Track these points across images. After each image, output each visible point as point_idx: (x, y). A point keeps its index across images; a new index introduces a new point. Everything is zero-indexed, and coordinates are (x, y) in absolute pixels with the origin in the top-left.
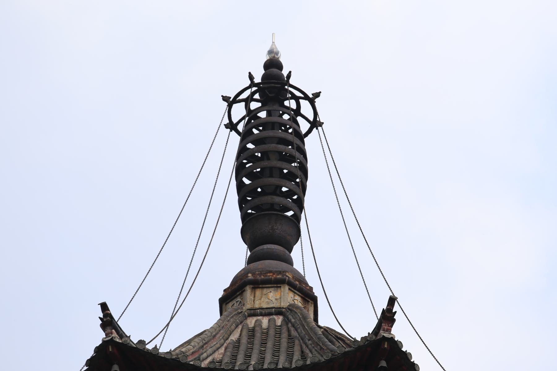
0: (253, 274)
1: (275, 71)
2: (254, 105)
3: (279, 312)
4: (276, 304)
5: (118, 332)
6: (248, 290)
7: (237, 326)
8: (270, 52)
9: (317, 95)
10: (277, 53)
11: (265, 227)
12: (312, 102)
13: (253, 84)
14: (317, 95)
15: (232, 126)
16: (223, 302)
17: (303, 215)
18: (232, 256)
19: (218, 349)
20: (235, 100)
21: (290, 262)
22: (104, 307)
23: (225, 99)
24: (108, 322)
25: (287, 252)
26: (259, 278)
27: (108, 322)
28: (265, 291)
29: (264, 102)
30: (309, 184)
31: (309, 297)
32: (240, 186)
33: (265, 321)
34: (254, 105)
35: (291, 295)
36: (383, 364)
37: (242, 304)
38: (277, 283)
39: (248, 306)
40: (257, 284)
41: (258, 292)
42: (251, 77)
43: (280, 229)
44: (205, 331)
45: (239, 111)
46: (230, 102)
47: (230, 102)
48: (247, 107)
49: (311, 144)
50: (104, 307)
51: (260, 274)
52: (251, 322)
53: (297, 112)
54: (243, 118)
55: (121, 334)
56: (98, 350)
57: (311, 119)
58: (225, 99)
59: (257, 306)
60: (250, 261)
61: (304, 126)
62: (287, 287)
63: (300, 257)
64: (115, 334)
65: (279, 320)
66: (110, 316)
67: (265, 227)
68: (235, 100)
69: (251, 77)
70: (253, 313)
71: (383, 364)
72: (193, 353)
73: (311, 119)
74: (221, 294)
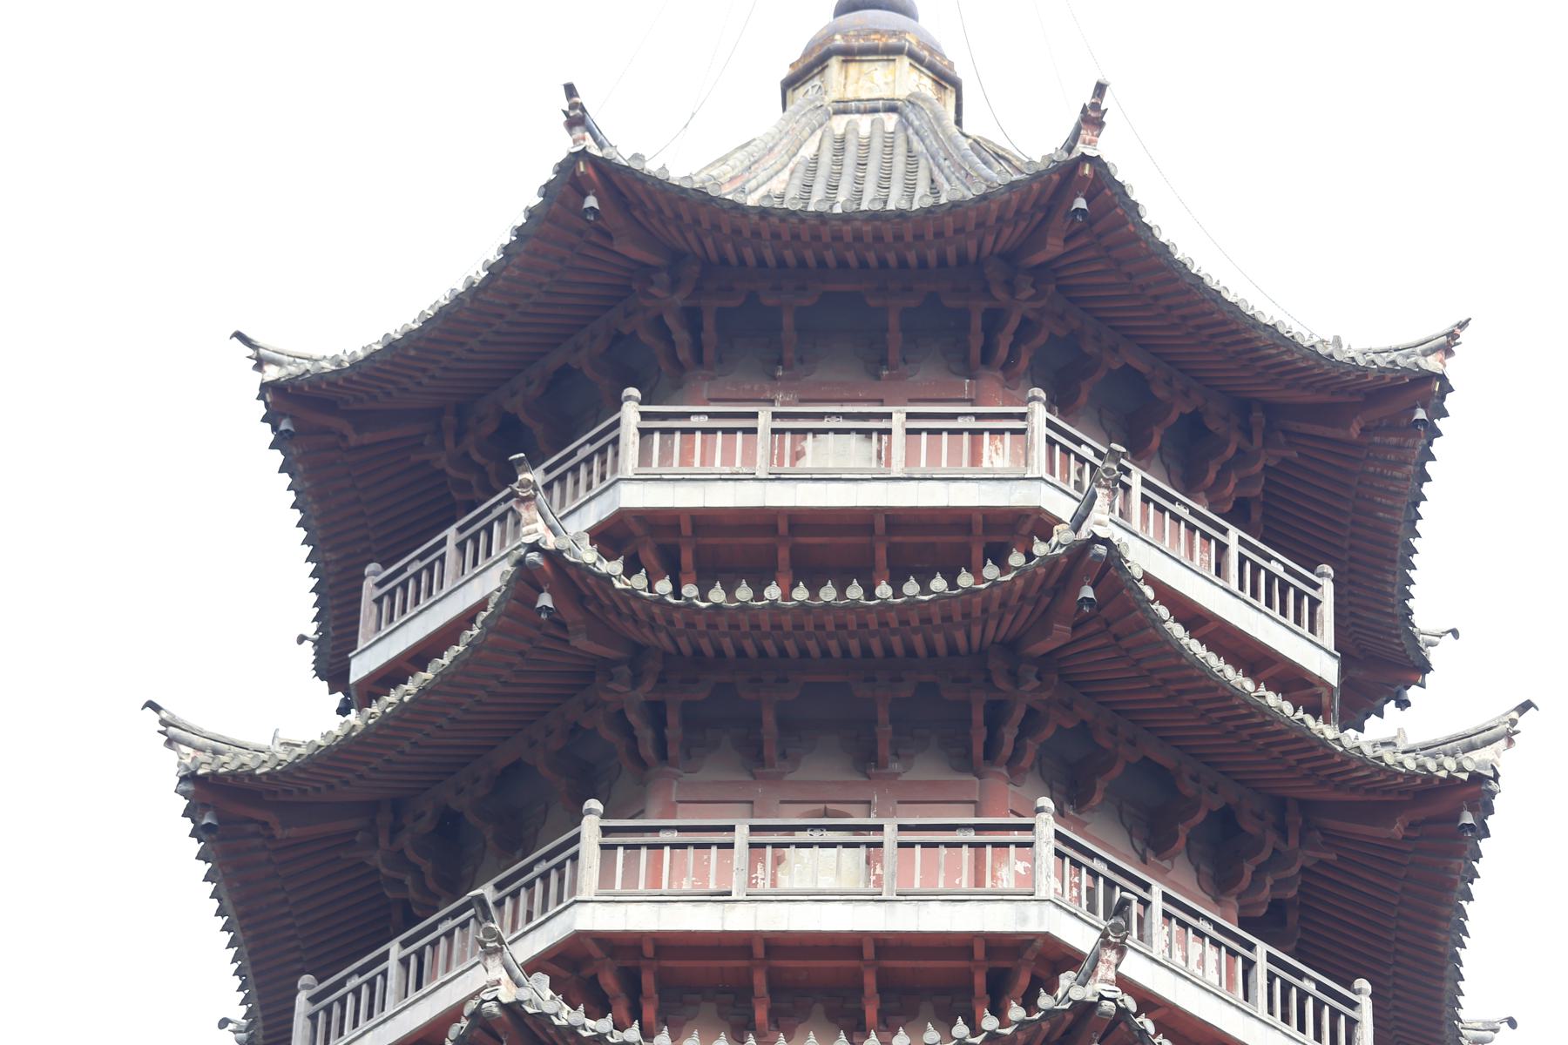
0: (845, 36)
6: (835, 63)
22: (570, 90)
33: (864, 123)
35: (915, 74)
38: (890, 52)
40: (850, 55)
41: (853, 69)
51: (858, 36)
52: (839, 124)
56: (547, 190)
59: (850, 95)
65: (891, 121)
70: (842, 108)
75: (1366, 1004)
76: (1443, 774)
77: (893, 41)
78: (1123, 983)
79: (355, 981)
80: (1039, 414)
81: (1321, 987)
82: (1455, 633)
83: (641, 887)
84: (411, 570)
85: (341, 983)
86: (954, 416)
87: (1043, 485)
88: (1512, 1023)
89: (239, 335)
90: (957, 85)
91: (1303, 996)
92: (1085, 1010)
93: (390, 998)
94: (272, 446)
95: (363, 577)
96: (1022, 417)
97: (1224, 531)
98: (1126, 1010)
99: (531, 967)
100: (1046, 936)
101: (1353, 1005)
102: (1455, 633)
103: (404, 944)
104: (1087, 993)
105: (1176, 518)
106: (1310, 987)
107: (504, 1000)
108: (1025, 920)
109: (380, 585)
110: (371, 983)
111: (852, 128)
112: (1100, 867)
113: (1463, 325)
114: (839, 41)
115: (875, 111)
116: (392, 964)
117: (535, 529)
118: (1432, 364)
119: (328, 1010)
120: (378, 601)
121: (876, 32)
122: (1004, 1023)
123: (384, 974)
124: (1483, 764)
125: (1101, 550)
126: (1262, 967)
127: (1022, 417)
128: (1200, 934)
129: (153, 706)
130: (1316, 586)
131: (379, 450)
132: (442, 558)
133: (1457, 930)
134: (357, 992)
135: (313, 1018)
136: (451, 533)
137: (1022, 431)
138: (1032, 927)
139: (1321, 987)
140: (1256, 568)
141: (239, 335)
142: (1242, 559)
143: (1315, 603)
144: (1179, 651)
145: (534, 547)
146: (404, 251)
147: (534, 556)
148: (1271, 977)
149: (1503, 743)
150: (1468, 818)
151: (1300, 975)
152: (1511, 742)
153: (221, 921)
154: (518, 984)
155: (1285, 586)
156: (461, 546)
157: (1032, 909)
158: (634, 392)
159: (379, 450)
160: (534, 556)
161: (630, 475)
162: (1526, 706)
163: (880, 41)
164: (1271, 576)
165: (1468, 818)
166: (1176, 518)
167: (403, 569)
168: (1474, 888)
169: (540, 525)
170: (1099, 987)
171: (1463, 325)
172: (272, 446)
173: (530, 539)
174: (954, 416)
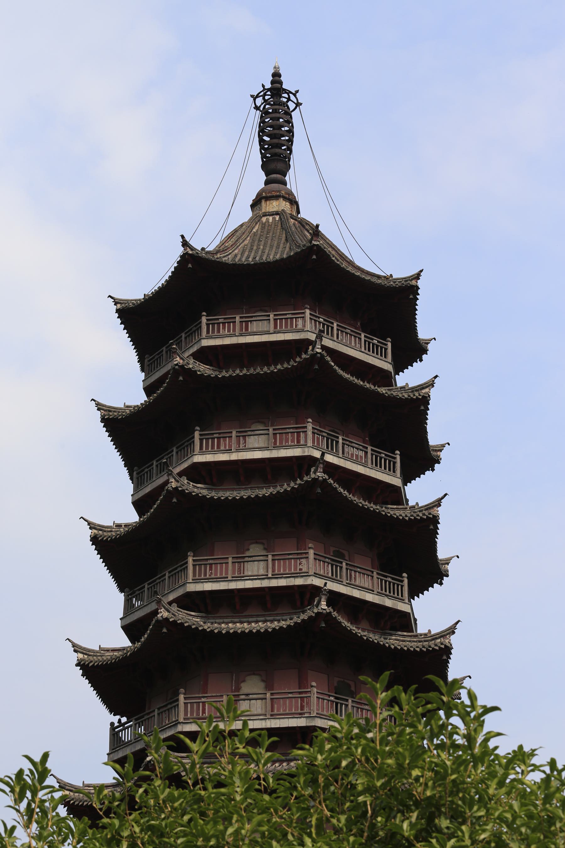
0: (265, 193)
1: (277, 78)
2: (267, 97)
3: (277, 213)
4: (275, 209)
5: (190, 248)
6: (263, 201)
7: (256, 224)
8: (275, 67)
9: (297, 92)
10: (278, 68)
11: (272, 166)
12: (295, 95)
13: (264, 89)
14: (297, 92)
15: (257, 108)
16: (253, 206)
17: (291, 156)
18: (257, 180)
19: (246, 239)
20: (258, 96)
21: (285, 184)
22: (183, 237)
23: (252, 96)
24: (185, 244)
25: (283, 177)
26: (268, 195)
27: (185, 244)
28: (271, 202)
29: (272, 96)
30: (295, 139)
31: (294, 202)
32: (261, 141)
33: (271, 218)
34: (267, 97)
35: (284, 202)
36: (314, 257)
37: (261, 210)
38: (277, 197)
39: (263, 211)
40: (267, 199)
41: (268, 202)
42: (263, 86)
43: (280, 166)
44: (242, 226)
45: (259, 101)
46: (255, 98)
47: (255, 98)
48: (264, 99)
49: (295, 115)
50: (183, 237)
51: (269, 193)
52: (264, 219)
53: (289, 99)
54: (262, 104)
55: (192, 249)
56: (181, 257)
57: (296, 102)
58: (252, 96)
59: (267, 210)
60: (267, 183)
61: (291, 106)
62: (282, 199)
63: (290, 178)
64: (188, 250)
65: (277, 218)
66: (186, 241)
67: (272, 166)
68: (258, 96)
69: (263, 86)
70: (265, 215)
71: (314, 257)
72: (232, 246)
73: (296, 102)
74: (251, 202)
75: (398, 457)
76: (415, 397)
77: (278, 194)
79: (146, 470)
80: (308, 312)
81: (386, 455)
82: (435, 339)
83: (210, 449)
84: (156, 358)
85: (143, 470)
86: (286, 314)
87: (309, 333)
88: (449, 444)
89: (110, 296)
90: (297, 203)
91: (381, 458)
92: (318, 614)
93: (154, 475)
94: (121, 324)
95: (145, 359)
96: (304, 313)
98: (326, 479)
99: (180, 474)
100: (310, 456)
102: (435, 339)
105: (347, 333)
106: (390, 579)
107: (173, 487)
108: (304, 452)
109: (149, 361)
110: (150, 470)
111: (268, 220)
112: (324, 434)
113: (421, 271)
114: (264, 194)
115: (273, 215)
116: (154, 466)
118: (414, 283)
119: (141, 477)
120: (149, 365)
121: (274, 191)
122: (296, 484)
123: (153, 468)
124: (425, 393)
125: (319, 355)
127: (304, 313)
128: (353, 447)
129: (93, 400)
130: (386, 345)
131: (150, 323)
132: (162, 355)
133: (426, 432)
134: (147, 472)
135: (138, 478)
136: (164, 348)
137: (304, 317)
138: (306, 454)
139: (386, 455)
140: (369, 343)
141: (110, 296)
142: (365, 341)
143: (402, 586)
144: (341, 376)
145: (177, 365)
146: (148, 276)
147: (177, 367)
148: (372, 455)
149: (431, 387)
150: (445, 657)
151: (386, 577)
152: (433, 386)
153: (116, 450)
154: (178, 481)
155: (377, 346)
156: (167, 352)
157: (306, 449)
158: (204, 313)
159: (150, 323)
160: (177, 367)
161: (204, 337)
162: (436, 377)
163: (274, 194)
164: (373, 344)
165: (422, 408)
166: (347, 333)
167: (154, 358)
168: (427, 421)
169: (178, 359)
171: (421, 271)
172: (121, 324)
173: (176, 363)
174: (286, 314)
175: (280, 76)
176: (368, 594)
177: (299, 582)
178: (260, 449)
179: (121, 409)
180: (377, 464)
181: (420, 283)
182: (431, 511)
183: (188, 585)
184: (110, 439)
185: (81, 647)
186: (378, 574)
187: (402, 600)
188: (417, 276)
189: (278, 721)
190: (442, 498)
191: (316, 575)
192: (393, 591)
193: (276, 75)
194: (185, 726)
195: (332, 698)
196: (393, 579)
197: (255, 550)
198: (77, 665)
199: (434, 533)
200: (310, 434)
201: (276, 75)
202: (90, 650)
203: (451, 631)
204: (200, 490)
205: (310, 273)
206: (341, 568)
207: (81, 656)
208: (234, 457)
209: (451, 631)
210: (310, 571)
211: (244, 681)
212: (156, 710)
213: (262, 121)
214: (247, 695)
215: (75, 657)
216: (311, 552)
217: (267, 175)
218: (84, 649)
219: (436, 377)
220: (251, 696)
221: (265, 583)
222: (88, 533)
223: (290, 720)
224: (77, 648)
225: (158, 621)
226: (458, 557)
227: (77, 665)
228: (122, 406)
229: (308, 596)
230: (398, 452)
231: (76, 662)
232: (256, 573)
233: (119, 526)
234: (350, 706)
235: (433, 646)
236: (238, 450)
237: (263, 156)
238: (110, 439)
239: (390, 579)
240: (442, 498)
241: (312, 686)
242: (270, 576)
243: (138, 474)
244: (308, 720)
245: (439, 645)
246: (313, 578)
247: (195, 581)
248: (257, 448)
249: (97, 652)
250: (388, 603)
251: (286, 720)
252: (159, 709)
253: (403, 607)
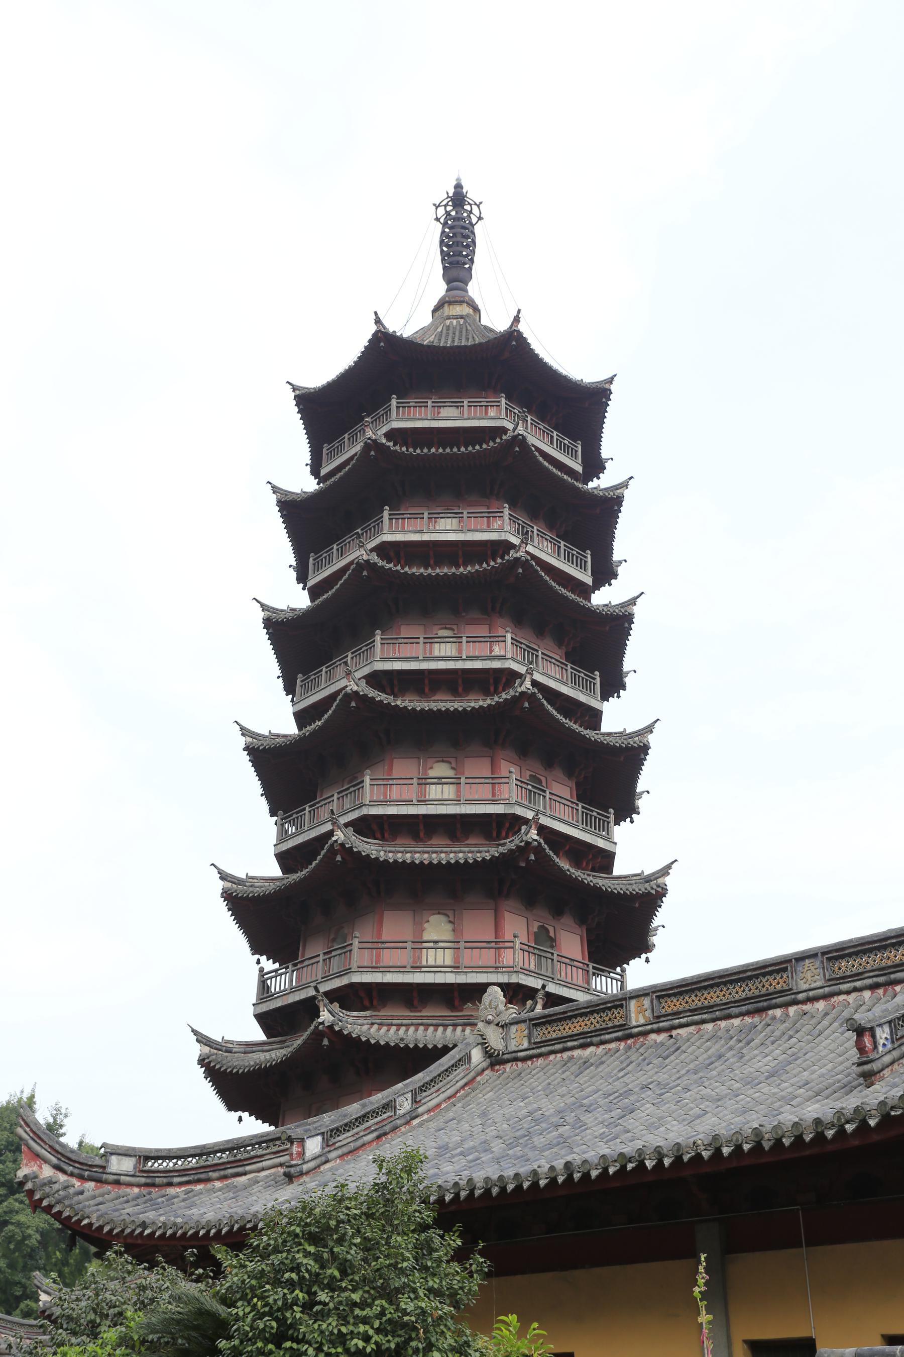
3: (462, 317)
6: (446, 305)
9: (481, 203)
12: (478, 206)
13: (448, 197)
14: (481, 203)
15: (437, 219)
16: (434, 311)
18: (439, 288)
21: (466, 291)
22: (376, 313)
23: (434, 205)
24: (378, 321)
27: (378, 321)
31: (476, 310)
32: (442, 251)
33: (455, 322)
40: (450, 303)
41: (451, 307)
45: (441, 211)
46: (437, 207)
49: (477, 229)
50: (376, 313)
52: (448, 322)
56: (374, 335)
58: (434, 205)
61: (474, 220)
65: (462, 321)
70: (449, 318)
75: (589, 557)
78: (535, 683)
80: (504, 401)
82: (648, 792)
90: (479, 311)
91: (573, 555)
92: (522, 693)
97: (566, 665)
101: (594, 679)
103: (310, 806)
104: (523, 688)
113: (615, 376)
117: (369, 433)
118: (607, 386)
126: (563, 547)
131: (326, 412)
133: (612, 537)
136: (346, 435)
143: (594, 684)
145: (369, 439)
146: (330, 359)
151: (579, 672)
157: (503, 534)
162: (632, 478)
165: (642, 756)
170: (521, 554)
171: (615, 376)
175: (462, 188)
176: (563, 686)
177: (496, 665)
178: (454, 531)
179: (297, 494)
180: (569, 558)
181: (613, 387)
182: (626, 608)
183: (375, 663)
184: (284, 525)
185: (249, 731)
186: (572, 668)
187: (595, 698)
188: (611, 380)
189: (473, 806)
190: (638, 597)
191: (513, 659)
192: (588, 688)
193: (458, 186)
194: (370, 808)
195: (530, 787)
196: (586, 675)
197: (441, 770)
198: (244, 750)
199: (624, 633)
200: (506, 518)
201: (458, 186)
202: (259, 735)
203: (649, 729)
204: (370, 848)
205: (506, 365)
206: (537, 656)
207: (249, 740)
208: (426, 537)
209: (649, 729)
210: (500, 527)
211: (431, 768)
212: (336, 795)
213: (443, 232)
214: (436, 942)
215: (242, 741)
216: (509, 636)
217: (448, 284)
218: (254, 733)
219: (632, 478)
220: (441, 944)
221: (459, 665)
222: (260, 615)
223: (487, 806)
224: (245, 732)
225: (346, 695)
226: (648, 792)
227: (244, 750)
228: (267, 734)
229: (504, 680)
230: (597, 673)
231: (244, 746)
232: (445, 651)
233: (293, 610)
234: (555, 961)
235: (649, 889)
236: (430, 532)
237: (444, 268)
238: (284, 525)
239: (582, 675)
240: (638, 597)
241: (510, 772)
242: (464, 657)
243: (314, 560)
244: (508, 807)
245: (655, 887)
246: (511, 661)
247: (383, 659)
248: (447, 529)
249: (267, 737)
250: (582, 698)
251: (483, 806)
252: (338, 793)
253: (594, 703)
